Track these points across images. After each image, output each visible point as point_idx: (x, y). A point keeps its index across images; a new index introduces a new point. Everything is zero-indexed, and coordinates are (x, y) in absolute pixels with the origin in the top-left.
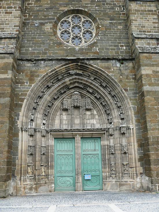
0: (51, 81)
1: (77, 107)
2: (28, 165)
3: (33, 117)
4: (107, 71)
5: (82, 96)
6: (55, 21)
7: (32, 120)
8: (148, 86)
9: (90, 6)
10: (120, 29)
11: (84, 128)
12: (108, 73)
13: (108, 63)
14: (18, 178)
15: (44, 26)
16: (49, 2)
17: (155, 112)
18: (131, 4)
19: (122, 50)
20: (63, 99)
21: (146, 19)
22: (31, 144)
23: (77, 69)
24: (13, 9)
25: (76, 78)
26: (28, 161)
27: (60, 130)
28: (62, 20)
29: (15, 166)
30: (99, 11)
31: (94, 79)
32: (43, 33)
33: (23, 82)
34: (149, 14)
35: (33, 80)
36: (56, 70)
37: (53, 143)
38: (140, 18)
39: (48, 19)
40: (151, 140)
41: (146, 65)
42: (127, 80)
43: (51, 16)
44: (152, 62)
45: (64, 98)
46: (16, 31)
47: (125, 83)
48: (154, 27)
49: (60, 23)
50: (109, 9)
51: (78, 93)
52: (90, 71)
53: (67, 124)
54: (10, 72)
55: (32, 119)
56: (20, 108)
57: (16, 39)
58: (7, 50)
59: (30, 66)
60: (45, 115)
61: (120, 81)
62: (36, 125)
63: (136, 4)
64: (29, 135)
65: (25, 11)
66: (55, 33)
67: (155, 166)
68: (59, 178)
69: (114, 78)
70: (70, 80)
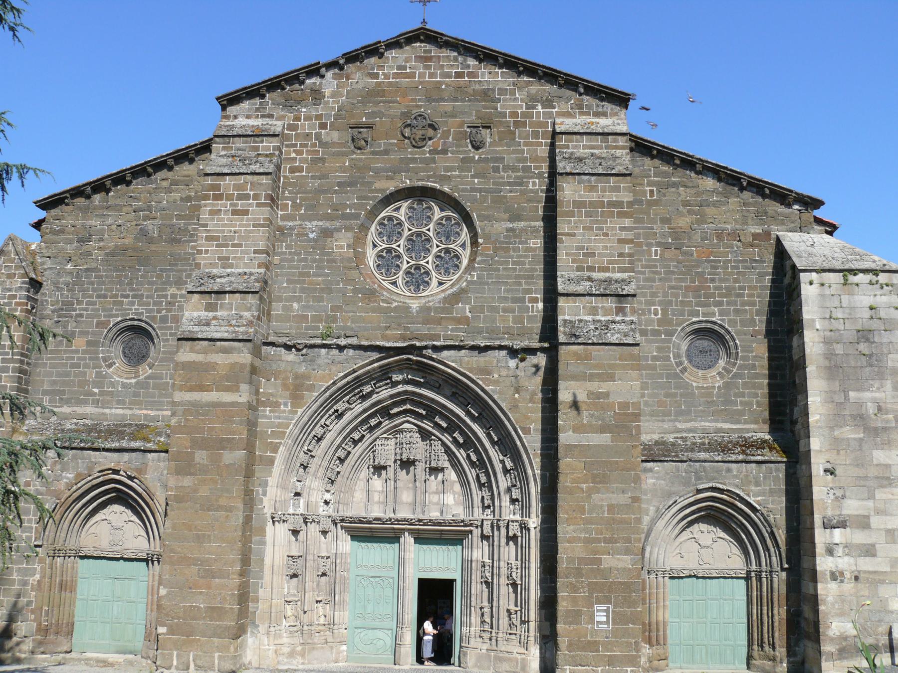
1: (407, 464)
2: (286, 599)
4: (482, 380)
5: (425, 435)
6: (362, 225)
7: (297, 494)
8: (571, 433)
9: (459, 176)
10: (534, 249)
13: (487, 359)
14: (262, 629)
15: (330, 239)
16: (347, 164)
18: (565, 185)
19: (533, 312)
20: (375, 440)
21: (601, 229)
22: (295, 553)
24: (251, 201)
25: (406, 392)
26: (286, 590)
27: (364, 518)
29: (258, 602)
30: (480, 190)
31: (451, 396)
32: (328, 261)
33: (277, 402)
34: (612, 215)
37: (348, 548)
38: (584, 228)
39: (345, 217)
41: (574, 378)
43: (350, 206)
44: (590, 370)
46: (259, 266)
48: (621, 255)
49: (374, 225)
50: (509, 184)
53: (382, 503)
54: (244, 387)
55: (298, 491)
56: (268, 467)
57: (257, 296)
58: (237, 329)
61: (514, 406)
62: (308, 506)
63: (579, 183)
64: (289, 530)
65: (283, 192)
66: (360, 258)
67: (567, 626)
68: (359, 630)
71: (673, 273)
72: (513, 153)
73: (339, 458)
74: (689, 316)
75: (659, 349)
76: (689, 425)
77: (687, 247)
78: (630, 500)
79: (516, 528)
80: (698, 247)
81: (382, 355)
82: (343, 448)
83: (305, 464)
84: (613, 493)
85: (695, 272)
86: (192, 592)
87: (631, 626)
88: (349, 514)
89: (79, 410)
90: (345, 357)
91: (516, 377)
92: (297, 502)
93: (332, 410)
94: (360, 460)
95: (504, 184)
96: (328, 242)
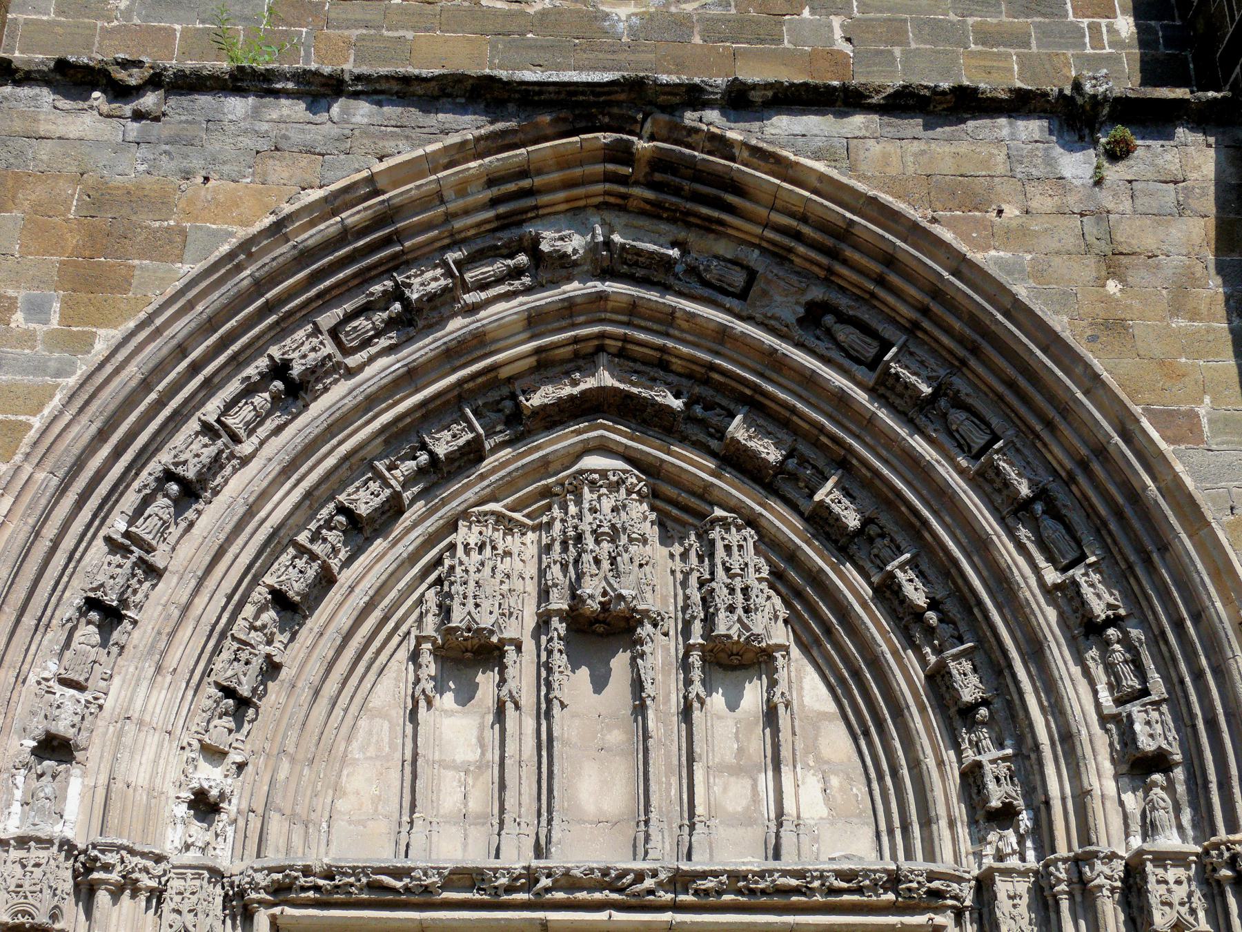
0: (327, 320)
3: (69, 706)
11: (685, 866)
12: (963, 248)
13: (964, 148)
20: (452, 526)
23: (620, 206)
27: (397, 873)
31: (801, 321)
35: (113, 289)
36: (376, 193)
42: (1180, 323)
45: (465, 515)
47: (1157, 350)
51: (620, 464)
52: (766, 225)
53: (481, 819)
55: (62, 727)
59: (90, 135)
60: (228, 692)
70: (535, 321)
73: (279, 599)
79: (1181, 892)
81: (500, 126)
82: (302, 550)
83: (112, 599)
88: (320, 858)
90: (335, 131)
91: (1101, 214)
92: (48, 787)
93: (262, 363)
94: (377, 615)
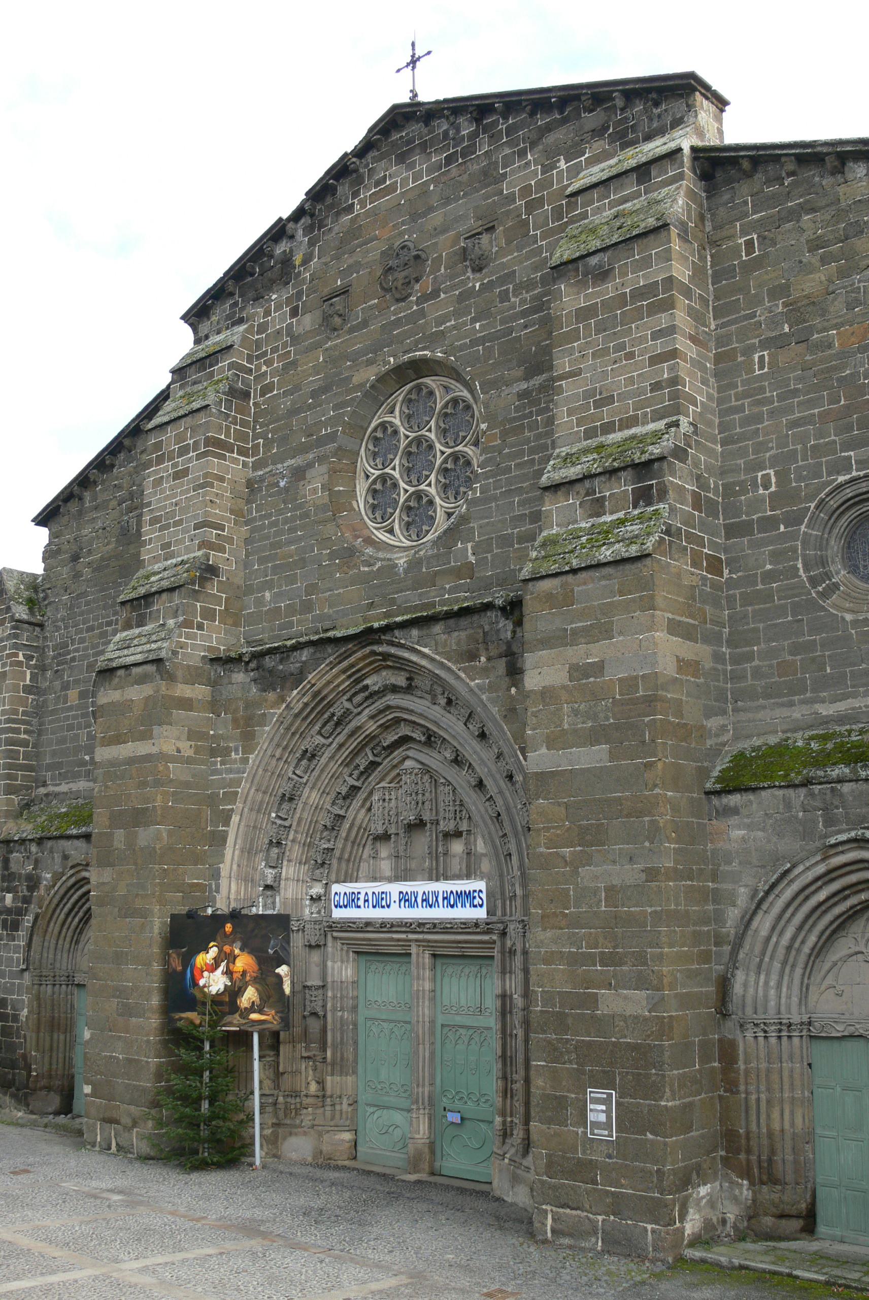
4: (464, 670)
8: (544, 750)
9: (454, 327)
15: (302, 483)
17: (564, 874)
21: (622, 347)
28: (373, 425)
34: (638, 314)
40: (539, 1008)
41: (546, 643)
44: (572, 623)
55: (269, 882)
67: (544, 1127)
68: (372, 1109)
69: (489, 699)
71: (795, 393)
72: (527, 259)
74: (829, 475)
75: (776, 556)
76: (842, 707)
77: (818, 333)
78: (643, 876)
80: (842, 324)
84: (614, 862)
85: (838, 380)
86: (112, 1036)
87: (650, 1136)
89: (74, 787)
95: (514, 318)
96: (301, 487)
